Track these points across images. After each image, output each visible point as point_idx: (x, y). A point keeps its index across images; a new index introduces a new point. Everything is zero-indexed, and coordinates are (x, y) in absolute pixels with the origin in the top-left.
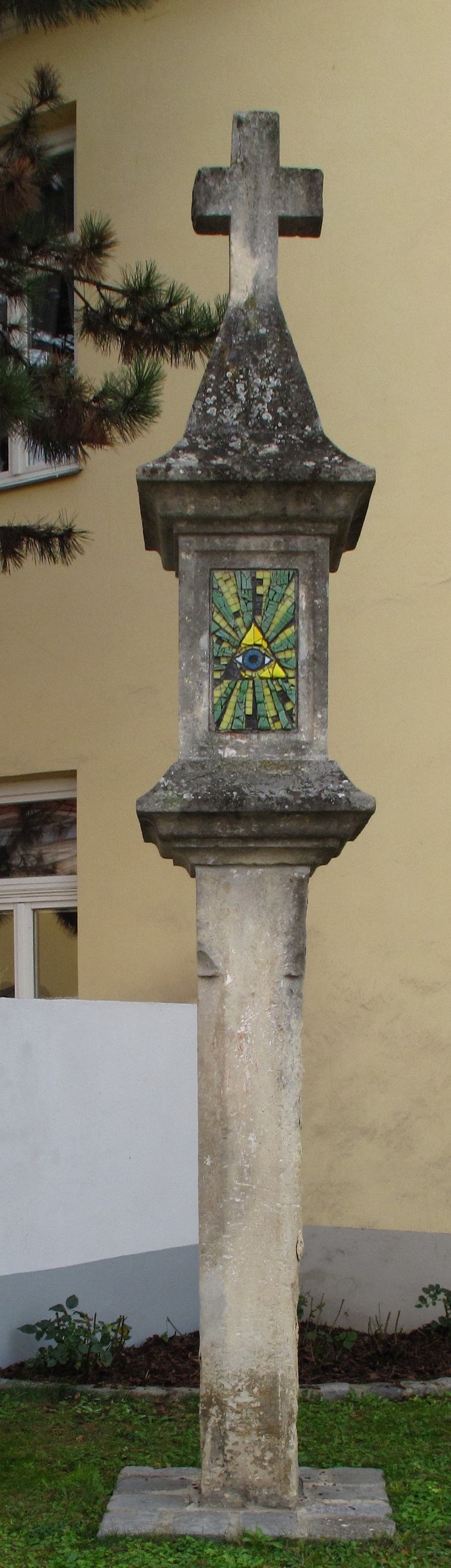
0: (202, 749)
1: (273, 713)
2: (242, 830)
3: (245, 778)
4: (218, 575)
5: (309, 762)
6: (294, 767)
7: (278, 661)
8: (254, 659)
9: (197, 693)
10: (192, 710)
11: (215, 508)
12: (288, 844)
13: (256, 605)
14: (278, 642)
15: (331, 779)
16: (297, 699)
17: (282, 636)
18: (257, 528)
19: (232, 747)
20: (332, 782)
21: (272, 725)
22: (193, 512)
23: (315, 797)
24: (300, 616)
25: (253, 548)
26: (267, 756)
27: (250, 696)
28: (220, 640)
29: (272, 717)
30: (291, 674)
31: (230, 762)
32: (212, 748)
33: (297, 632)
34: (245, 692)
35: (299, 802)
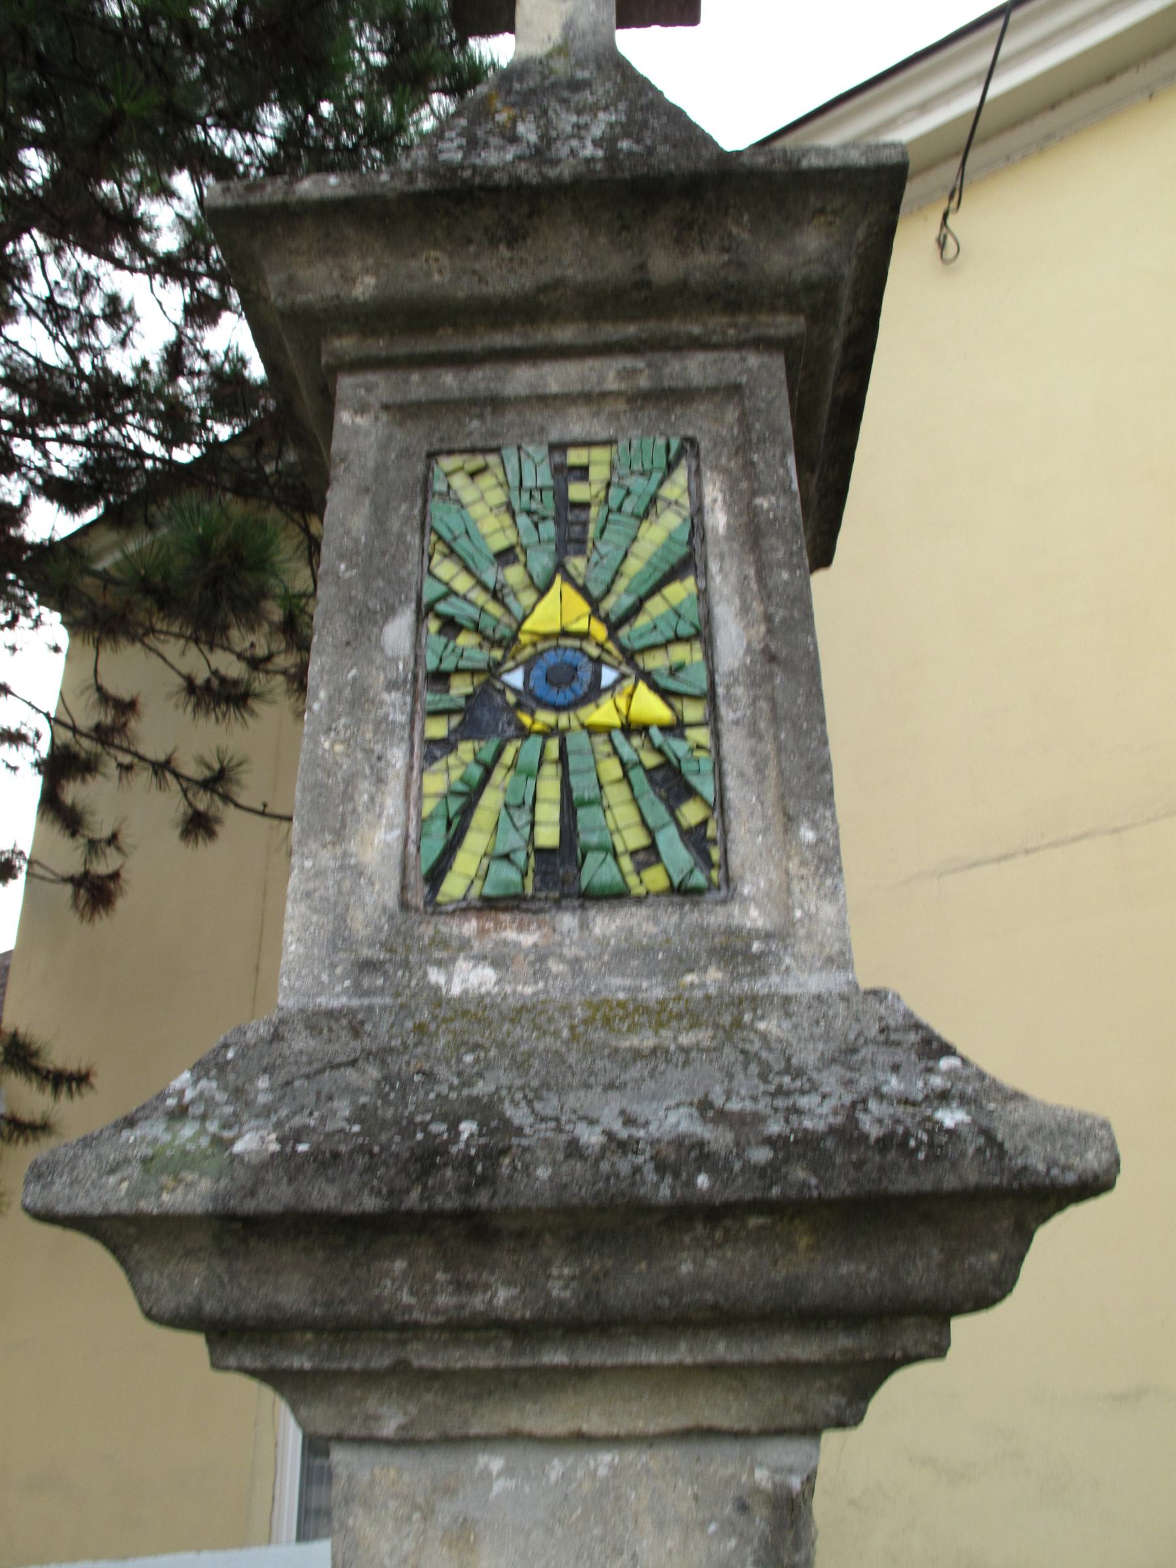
0: (368, 966)
1: (636, 839)
2: (503, 1295)
3: (521, 1065)
4: (447, 463)
5: (787, 999)
6: (726, 1019)
7: (646, 676)
8: (567, 677)
9: (365, 788)
10: (340, 835)
11: (436, 278)
12: (721, 1349)
13: (571, 529)
14: (642, 621)
15: (884, 1057)
16: (721, 791)
17: (656, 607)
18: (565, 334)
19: (480, 958)
20: (896, 1068)
21: (632, 880)
22: (370, 292)
23: (832, 1130)
24: (712, 550)
25: (554, 388)
26: (617, 986)
27: (549, 787)
28: (451, 626)
29: (633, 854)
30: (693, 712)
31: (474, 1010)
32: (406, 965)
33: (703, 595)
34: (534, 774)
35: (761, 1155)
